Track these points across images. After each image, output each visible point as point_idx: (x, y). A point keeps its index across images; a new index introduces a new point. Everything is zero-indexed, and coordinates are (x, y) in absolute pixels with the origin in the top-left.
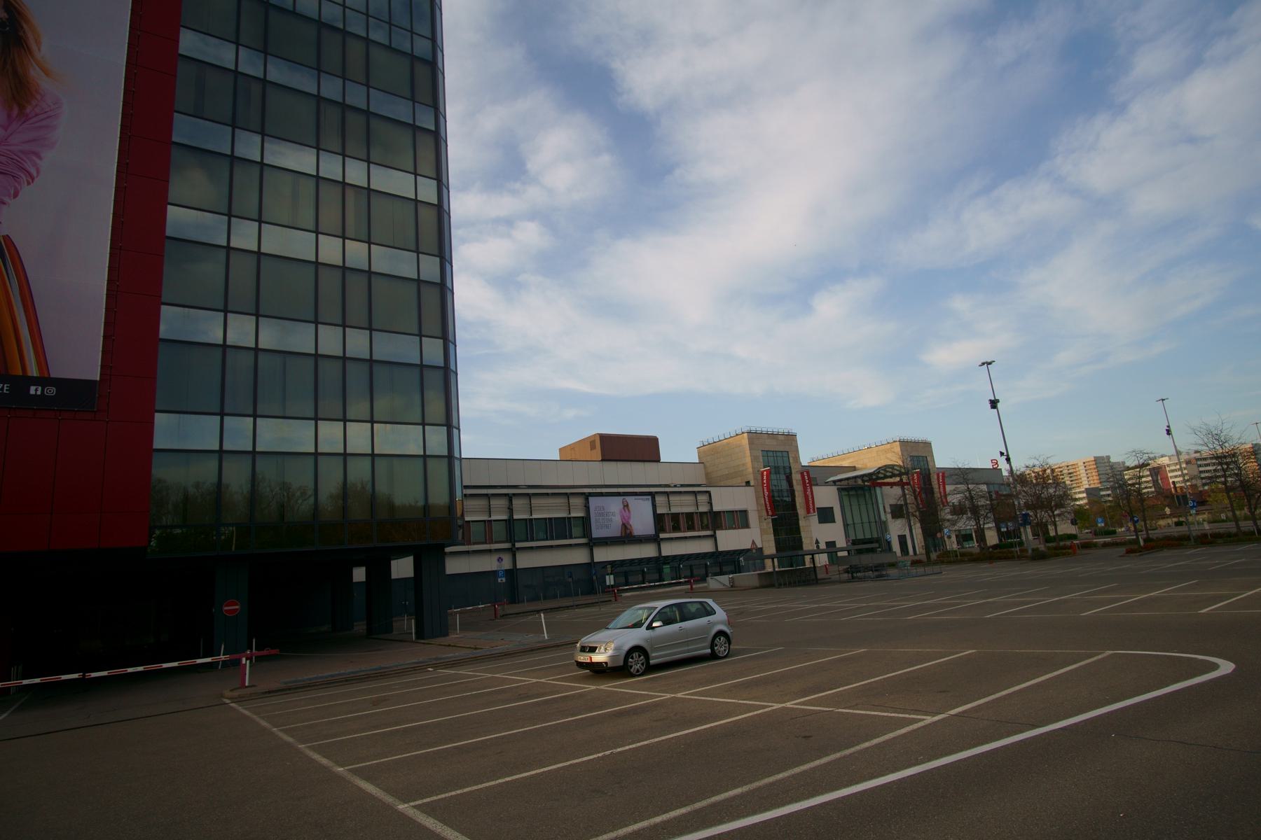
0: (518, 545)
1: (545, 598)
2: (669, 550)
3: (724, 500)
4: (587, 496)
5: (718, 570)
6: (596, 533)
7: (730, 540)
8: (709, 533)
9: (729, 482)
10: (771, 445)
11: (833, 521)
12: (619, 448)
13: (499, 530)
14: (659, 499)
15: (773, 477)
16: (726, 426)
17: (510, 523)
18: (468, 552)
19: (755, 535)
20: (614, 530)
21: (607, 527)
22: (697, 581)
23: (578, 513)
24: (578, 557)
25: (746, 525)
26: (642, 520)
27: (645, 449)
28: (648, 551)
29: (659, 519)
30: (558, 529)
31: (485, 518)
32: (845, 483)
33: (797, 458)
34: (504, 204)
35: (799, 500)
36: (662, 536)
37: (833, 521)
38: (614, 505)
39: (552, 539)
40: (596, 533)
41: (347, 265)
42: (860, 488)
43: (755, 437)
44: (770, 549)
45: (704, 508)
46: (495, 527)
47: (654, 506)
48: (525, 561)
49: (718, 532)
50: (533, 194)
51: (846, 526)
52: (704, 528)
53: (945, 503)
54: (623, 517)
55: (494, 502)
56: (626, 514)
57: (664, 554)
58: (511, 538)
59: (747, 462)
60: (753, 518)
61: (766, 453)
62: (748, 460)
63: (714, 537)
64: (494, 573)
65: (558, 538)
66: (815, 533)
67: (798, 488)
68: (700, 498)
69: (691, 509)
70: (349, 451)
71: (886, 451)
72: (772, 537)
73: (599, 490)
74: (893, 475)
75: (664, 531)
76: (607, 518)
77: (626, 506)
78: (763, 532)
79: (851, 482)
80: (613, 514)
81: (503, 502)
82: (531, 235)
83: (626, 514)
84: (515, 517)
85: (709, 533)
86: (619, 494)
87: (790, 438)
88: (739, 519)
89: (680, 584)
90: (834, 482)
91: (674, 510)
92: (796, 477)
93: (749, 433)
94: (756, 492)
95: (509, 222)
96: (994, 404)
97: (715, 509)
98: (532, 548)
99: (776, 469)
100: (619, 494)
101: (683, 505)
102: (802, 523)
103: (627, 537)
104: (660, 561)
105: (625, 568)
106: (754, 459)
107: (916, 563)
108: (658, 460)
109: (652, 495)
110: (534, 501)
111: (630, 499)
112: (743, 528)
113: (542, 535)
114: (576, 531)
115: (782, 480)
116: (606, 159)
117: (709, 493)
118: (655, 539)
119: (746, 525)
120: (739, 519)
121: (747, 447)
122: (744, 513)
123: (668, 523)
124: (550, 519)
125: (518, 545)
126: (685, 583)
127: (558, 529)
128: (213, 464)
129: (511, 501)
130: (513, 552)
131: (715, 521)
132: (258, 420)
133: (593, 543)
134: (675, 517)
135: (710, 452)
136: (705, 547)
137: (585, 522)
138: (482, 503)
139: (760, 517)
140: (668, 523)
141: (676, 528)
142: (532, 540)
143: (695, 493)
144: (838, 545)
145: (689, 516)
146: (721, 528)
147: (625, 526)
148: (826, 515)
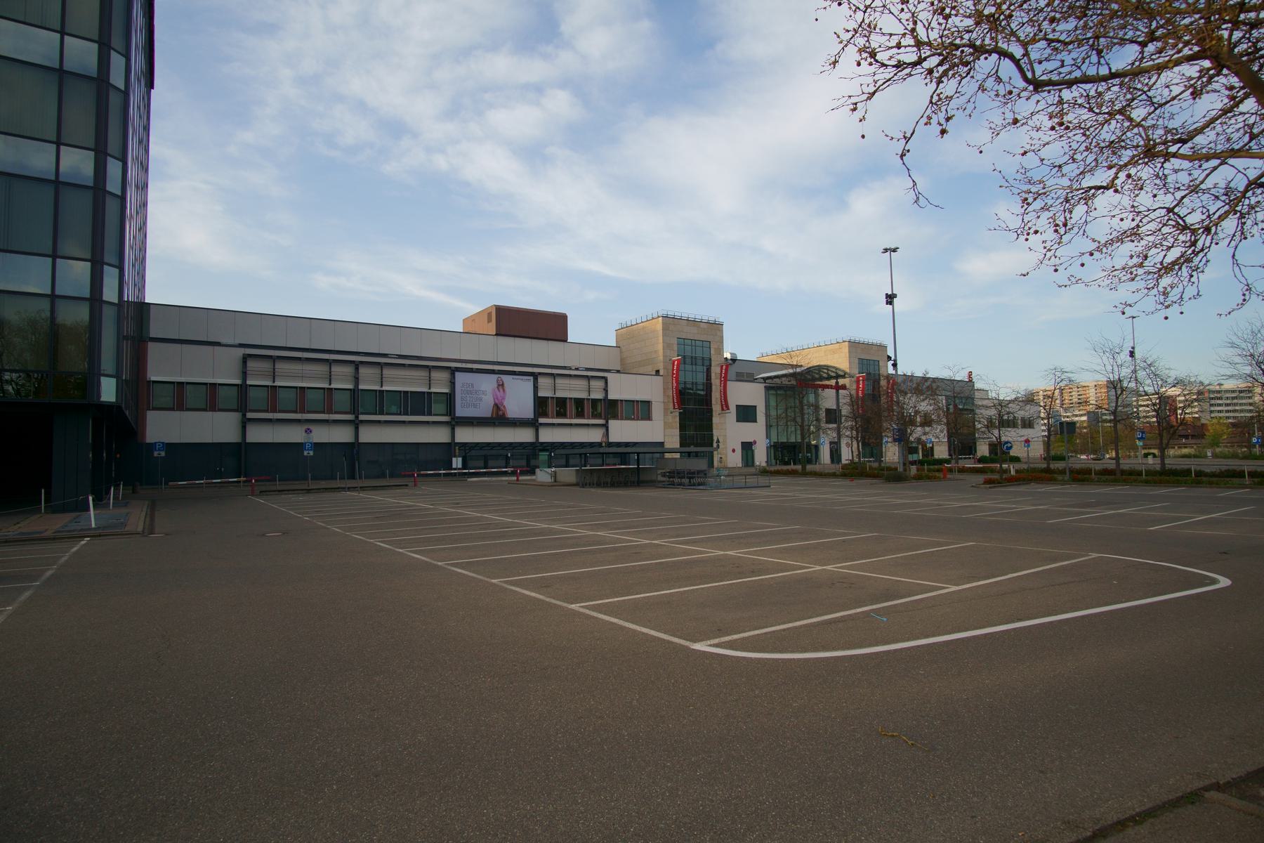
0: (362, 417)
1: (392, 476)
2: (547, 436)
3: (620, 389)
4: (453, 371)
5: (563, 462)
6: (460, 412)
7: (623, 431)
8: (601, 422)
9: (641, 370)
10: (692, 333)
11: (755, 421)
12: (512, 322)
13: (343, 401)
14: (541, 380)
15: (682, 367)
16: (643, 310)
17: (355, 393)
18: (327, 421)
19: (660, 429)
20: (485, 410)
22: (523, 473)
23: (441, 388)
24: (439, 436)
25: (648, 417)
26: (519, 400)
27: (550, 326)
28: (524, 436)
29: (541, 404)
31: (269, 383)
32: (777, 380)
33: (720, 350)
34: (534, 69)
35: (716, 395)
36: (542, 420)
37: (755, 421)
38: (487, 384)
40: (460, 412)
41: (68, 66)
42: (795, 387)
43: (670, 321)
44: (673, 441)
45: (598, 395)
46: (336, 396)
48: (369, 435)
49: (612, 423)
51: (769, 427)
52: (594, 416)
54: (495, 397)
55: (435, 374)
56: (500, 394)
57: (541, 440)
58: (354, 410)
59: (659, 350)
60: (657, 411)
61: (682, 342)
62: (660, 347)
63: (606, 426)
64: (300, 446)
65: (412, 414)
66: (730, 435)
67: (716, 382)
68: (594, 383)
69: (583, 395)
70: (57, 293)
71: (834, 352)
72: (677, 432)
74: (829, 378)
75: (545, 415)
76: (477, 395)
77: (501, 385)
79: (785, 381)
80: (484, 393)
81: (445, 376)
82: (561, 104)
83: (500, 394)
84: (361, 387)
85: (601, 422)
86: (493, 372)
87: (716, 327)
88: (641, 410)
89: (505, 473)
90: (765, 379)
91: (559, 394)
92: (715, 370)
93: (665, 317)
94: (665, 383)
95: (537, 90)
96: (890, 299)
97: (610, 397)
98: (379, 422)
99: (694, 361)
100: (493, 372)
101: (571, 390)
102: (715, 420)
103: (499, 419)
104: (536, 448)
105: (583, 451)
106: (667, 346)
107: (764, 472)
108: (565, 340)
109: (535, 376)
110: (387, 372)
111: (506, 378)
112: (642, 419)
113: (394, 409)
114: (438, 407)
115: (696, 374)
116: (646, 25)
117: (605, 379)
118: (533, 424)
119: (648, 417)
120: (641, 410)
121: (661, 333)
122: (647, 404)
123: (551, 408)
124: (406, 393)
125: (362, 417)
127: (416, 404)
128: (45, 305)
129: (357, 369)
130: (356, 424)
131: (610, 409)
132: (58, 260)
133: (456, 422)
134: (562, 402)
135: (628, 335)
136: (594, 436)
137: (450, 399)
138: (266, 365)
139: (666, 409)
140: (551, 408)
141: (561, 414)
142: (382, 413)
143: (330, 363)
144: (667, 446)
145: (579, 402)
146: (615, 417)
147: (497, 407)
148: (746, 414)
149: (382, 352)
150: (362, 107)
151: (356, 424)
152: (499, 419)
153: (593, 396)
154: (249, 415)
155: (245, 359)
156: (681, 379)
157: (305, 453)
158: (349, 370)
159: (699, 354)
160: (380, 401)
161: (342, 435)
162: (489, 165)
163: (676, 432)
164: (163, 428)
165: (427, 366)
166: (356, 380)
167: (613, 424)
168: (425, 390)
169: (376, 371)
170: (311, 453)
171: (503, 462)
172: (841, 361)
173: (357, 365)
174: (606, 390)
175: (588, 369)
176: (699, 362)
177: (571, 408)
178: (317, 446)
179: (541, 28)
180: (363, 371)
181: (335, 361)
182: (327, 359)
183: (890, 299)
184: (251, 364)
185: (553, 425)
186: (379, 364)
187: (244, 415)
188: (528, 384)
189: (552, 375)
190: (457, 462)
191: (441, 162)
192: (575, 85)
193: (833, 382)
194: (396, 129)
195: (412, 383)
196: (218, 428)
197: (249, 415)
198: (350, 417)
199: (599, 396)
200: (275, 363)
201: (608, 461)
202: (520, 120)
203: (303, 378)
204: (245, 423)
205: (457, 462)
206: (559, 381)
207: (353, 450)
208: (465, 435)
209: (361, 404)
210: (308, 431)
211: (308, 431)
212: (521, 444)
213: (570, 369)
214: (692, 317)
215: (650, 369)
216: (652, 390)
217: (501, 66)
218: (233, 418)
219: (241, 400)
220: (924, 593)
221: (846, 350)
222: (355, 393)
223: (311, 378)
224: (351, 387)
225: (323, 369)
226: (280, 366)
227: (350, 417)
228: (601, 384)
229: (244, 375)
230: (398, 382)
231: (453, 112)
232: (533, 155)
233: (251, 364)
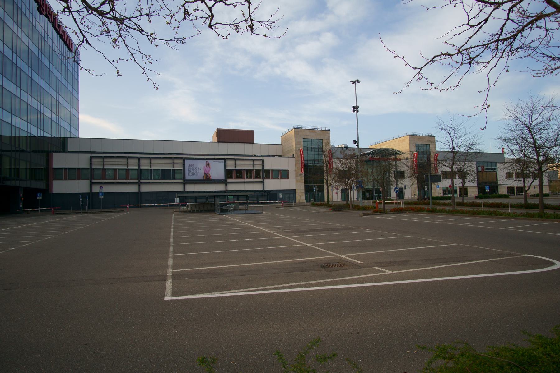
0: (142, 181)
2: (231, 187)
3: (270, 165)
4: (184, 159)
6: (188, 177)
7: (271, 185)
8: (261, 180)
12: (225, 136)
18: (114, 183)
19: (294, 183)
20: (200, 176)
21: (195, 175)
24: (178, 188)
26: (217, 170)
27: (246, 137)
28: (220, 187)
29: (229, 174)
30: (168, 174)
33: (328, 143)
34: (317, 25)
36: (229, 180)
38: (201, 165)
39: (162, 179)
40: (188, 177)
47: (225, 166)
48: (145, 189)
50: (331, 19)
52: (257, 178)
53: (330, 169)
54: (205, 170)
56: (207, 169)
60: (292, 174)
61: (306, 140)
63: (263, 183)
69: (251, 168)
72: (303, 184)
73: (190, 157)
75: (231, 177)
77: (208, 165)
78: (297, 181)
80: (199, 169)
81: (181, 161)
82: (329, 39)
83: (207, 169)
84: (141, 168)
85: (261, 180)
87: (326, 132)
88: (284, 174)
91: (237, 168)
95: (318, 34)
98: (161, 183)
99: (423, 153)
103: (207, 180)
106: (297, 143)
108: (253, 143)
109: (225, 160)
110: (153, 161)
111: (210, 161)
114: (179, 176)
117: (262, 160)
118: (224, 182)
120: (284, 174)
122: (287, 171)
123: (235, 174)
125: (142, 181)
126: (279, 203)
127: (168, 174)
129: (139, 160)
130: (139, 184)
131: (268, 174)
133: (186, 182)
134: (239, 172)
136: (258, 187)
137: (183, 171)
138: (100, 160)
139: (296, 174)
140: (235, 174)
143: (128, 158)
145: (248, 171)
147: (206, 175)
149: (162, 152)
150: (245, 52)
151: (139, 184)
152: (207, 180)
153: (256, 168)
154: (94, 181)
155: (91, 158)
156: (305, 157)
157: (38, 198)
158: (181, 161)
159: (316, 146)
160: (151, 174)
161: (133, 189)
162: (298, 70)
163: (303, 185)
164: (60, 187)
165: (172, 157)
166: (139, 165)
167: (266, 181)
168: (172, 168)
169: (149, 161)
170: (41, 198)
171: (245, 199)
172: (404, 147)
173: (139, 159)
174: (263, 166)
175: (104, 153)
176: (425, 153)
177: (244, 174)
178: (105, 194)
179: (319, 5)
180: (142, 161)
181: (237, 159)
182: (126, 156)
183: (356, 109)
184: (94, 160)
185: (234, 182)
186: (149, 157)
187: (91, 181)
188: (221, 165)
189: (234, 159)
190: (177, 200)
191: (278, 71)
192: (335, 30)
193: (393, 157)
194: (259, 59)
195: (166, 165)
196: (80, 187)
197: (94, 181)
198: (137, 181)
199: (260, 168)
200: (108, 158)
201: (209, 200)
202: (310, 48)
203: (116, 165)
204: (91, 184)
205: (177, 200)
206: (238, 162)
207: (92, 196)
208: (190, 188)
209: (142, 175)
210: (101, 188)
211: (101, 188)
212: (257, 191)
213: (251, 156)
214: (312, 128)
215: (291, 155)
216: (290, 165)
217: (302, 26)
218: (87, 182)
219: (89, 174)
220: (378, 268)
221: (408, 139)
222: (140, 171)
223: (119, 165)
224: (137, 168)
225: (125, 161)
226: (106, 160)
227: (137, 181)
228: (260, 162)
229: (91, 164)
230: (159, 165)
231: (281, 49)
232: (317, 63)
233: (94, 160)
